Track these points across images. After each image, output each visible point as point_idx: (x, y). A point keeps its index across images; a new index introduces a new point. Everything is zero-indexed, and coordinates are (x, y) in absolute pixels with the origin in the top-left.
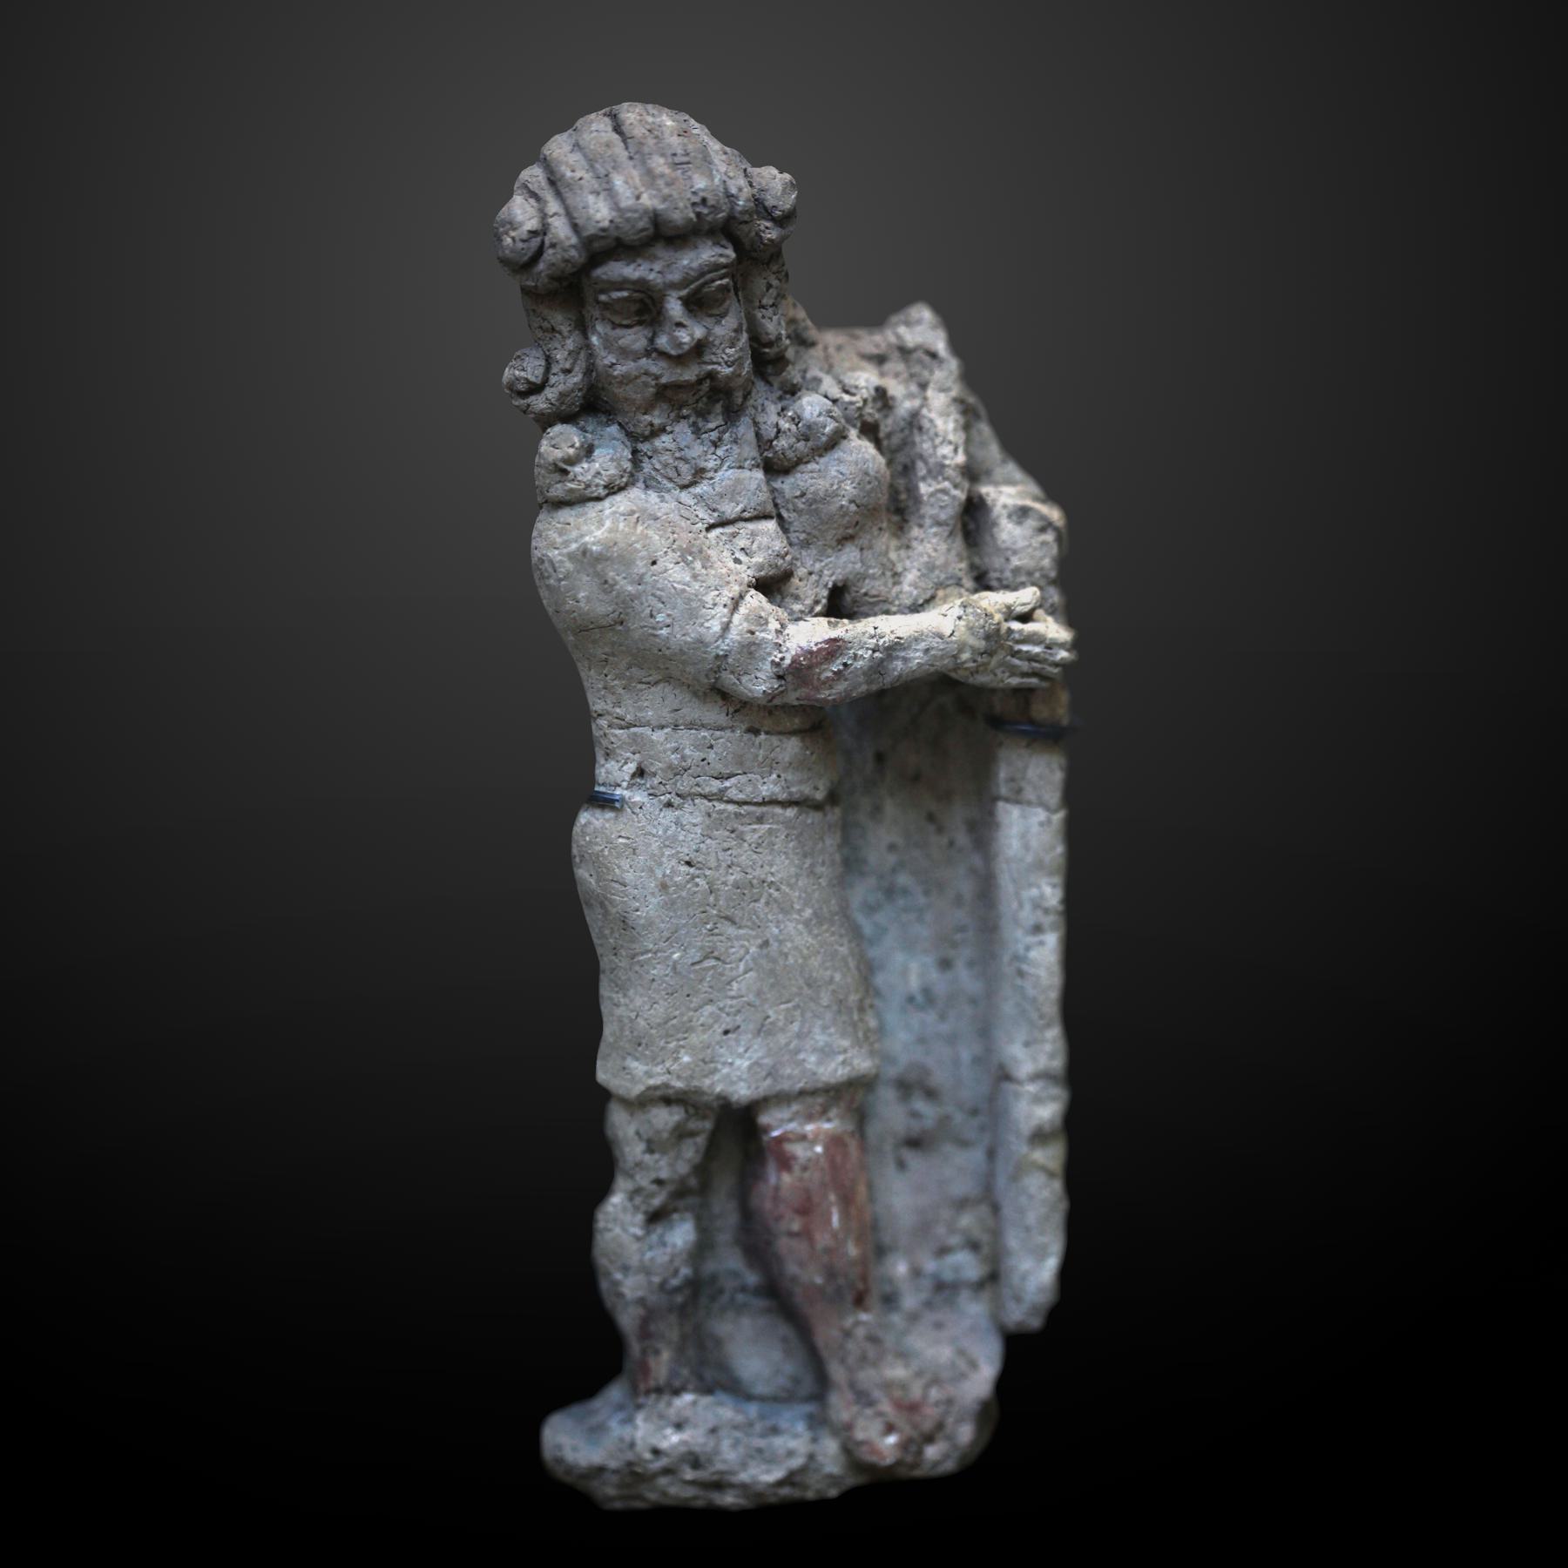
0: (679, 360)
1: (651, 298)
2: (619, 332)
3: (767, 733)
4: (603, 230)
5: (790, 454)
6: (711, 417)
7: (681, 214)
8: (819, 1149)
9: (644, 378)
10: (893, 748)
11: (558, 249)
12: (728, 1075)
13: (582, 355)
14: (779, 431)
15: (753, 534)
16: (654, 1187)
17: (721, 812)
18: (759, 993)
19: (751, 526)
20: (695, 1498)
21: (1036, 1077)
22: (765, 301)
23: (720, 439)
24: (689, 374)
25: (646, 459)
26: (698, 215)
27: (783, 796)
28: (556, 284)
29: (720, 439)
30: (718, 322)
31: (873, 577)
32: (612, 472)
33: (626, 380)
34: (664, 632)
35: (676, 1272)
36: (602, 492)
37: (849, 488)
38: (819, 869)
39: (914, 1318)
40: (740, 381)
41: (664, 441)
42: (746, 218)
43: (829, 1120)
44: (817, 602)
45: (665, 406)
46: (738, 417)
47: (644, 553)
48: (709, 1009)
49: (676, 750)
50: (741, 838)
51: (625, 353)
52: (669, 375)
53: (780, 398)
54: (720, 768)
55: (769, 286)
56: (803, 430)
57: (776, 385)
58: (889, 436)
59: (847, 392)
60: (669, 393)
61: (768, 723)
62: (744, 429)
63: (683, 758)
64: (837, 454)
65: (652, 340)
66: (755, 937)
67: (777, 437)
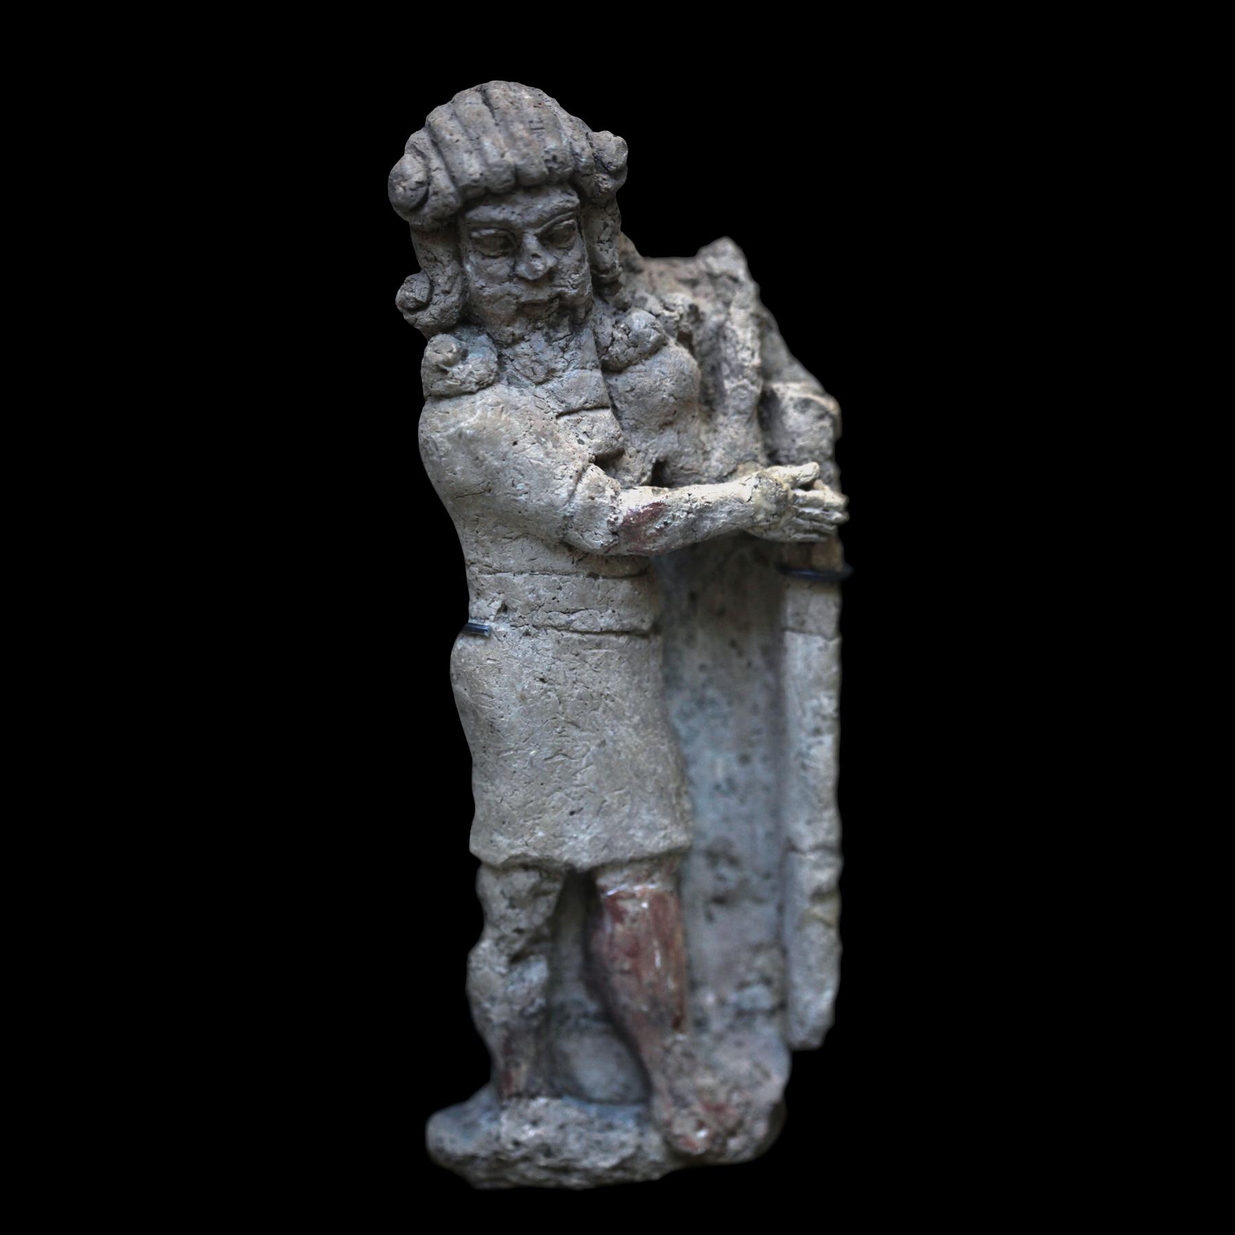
0: (535, 284)
1: (513, 234)
2: (488, 261)
3: (604, 577)
4: (475, 181)
5: (622, 358)
6: (560, 328)
7: (536, 168)
8: (645, 905)
9: (507, 298)
10: (698, 588)
11: (440, 196)
12: (573, 847)
13: (459, 279)
14: (613, 340)
15: (593, 421)
16: (515, 935)
17: (568, 640)
18: (598, 782)
19: (591, 414)
20: (548, 1180)
21: (816, 848)
22: (602, 237)
23: (567, 346)
24: (543, 295)
25: (509, 362)
26: (550, 169)
27: (616, 627)
28: (438, 224)
29: (567, 346)
30: (566, 254)
31: (688, 455)
32: (482, 371)
33: (493, 299)
34: (523, 498)
35: (533, 1002)
36: (474, 387)
37: (668, 384)
38: (645, 685)
39: (720, 1038)
40: (583, 300)
41: (523, 347)
42: (588, 171)
43: (653, 882)
44: (643, 474)
45: (524, 320)
46: (581, 329)
47: (507, 436)
48: (558, 794)
49: (532, 591)
50: (584, 660)
51: (492, 278)
52: (527, 295)
53: (615, 314)
54: (567, 605)
55: (606, 225)
56: (633, 339)
57: (611, 303)
58: (700, 343)
59: (667, 309)
60: (527, 310)
61: (605, 570)
62: (586, 338)
63: (538, 597)
64: (659, 357)
65: (513, 268)
66: (595, 738)
67: (612, 344)
